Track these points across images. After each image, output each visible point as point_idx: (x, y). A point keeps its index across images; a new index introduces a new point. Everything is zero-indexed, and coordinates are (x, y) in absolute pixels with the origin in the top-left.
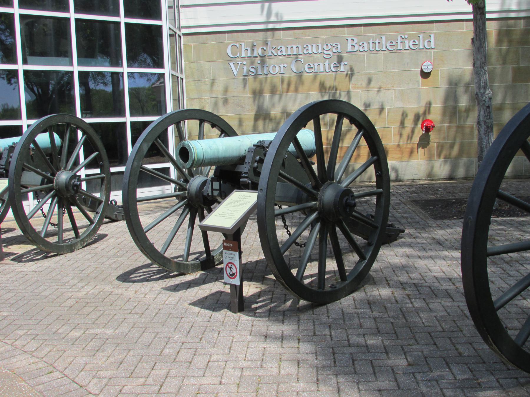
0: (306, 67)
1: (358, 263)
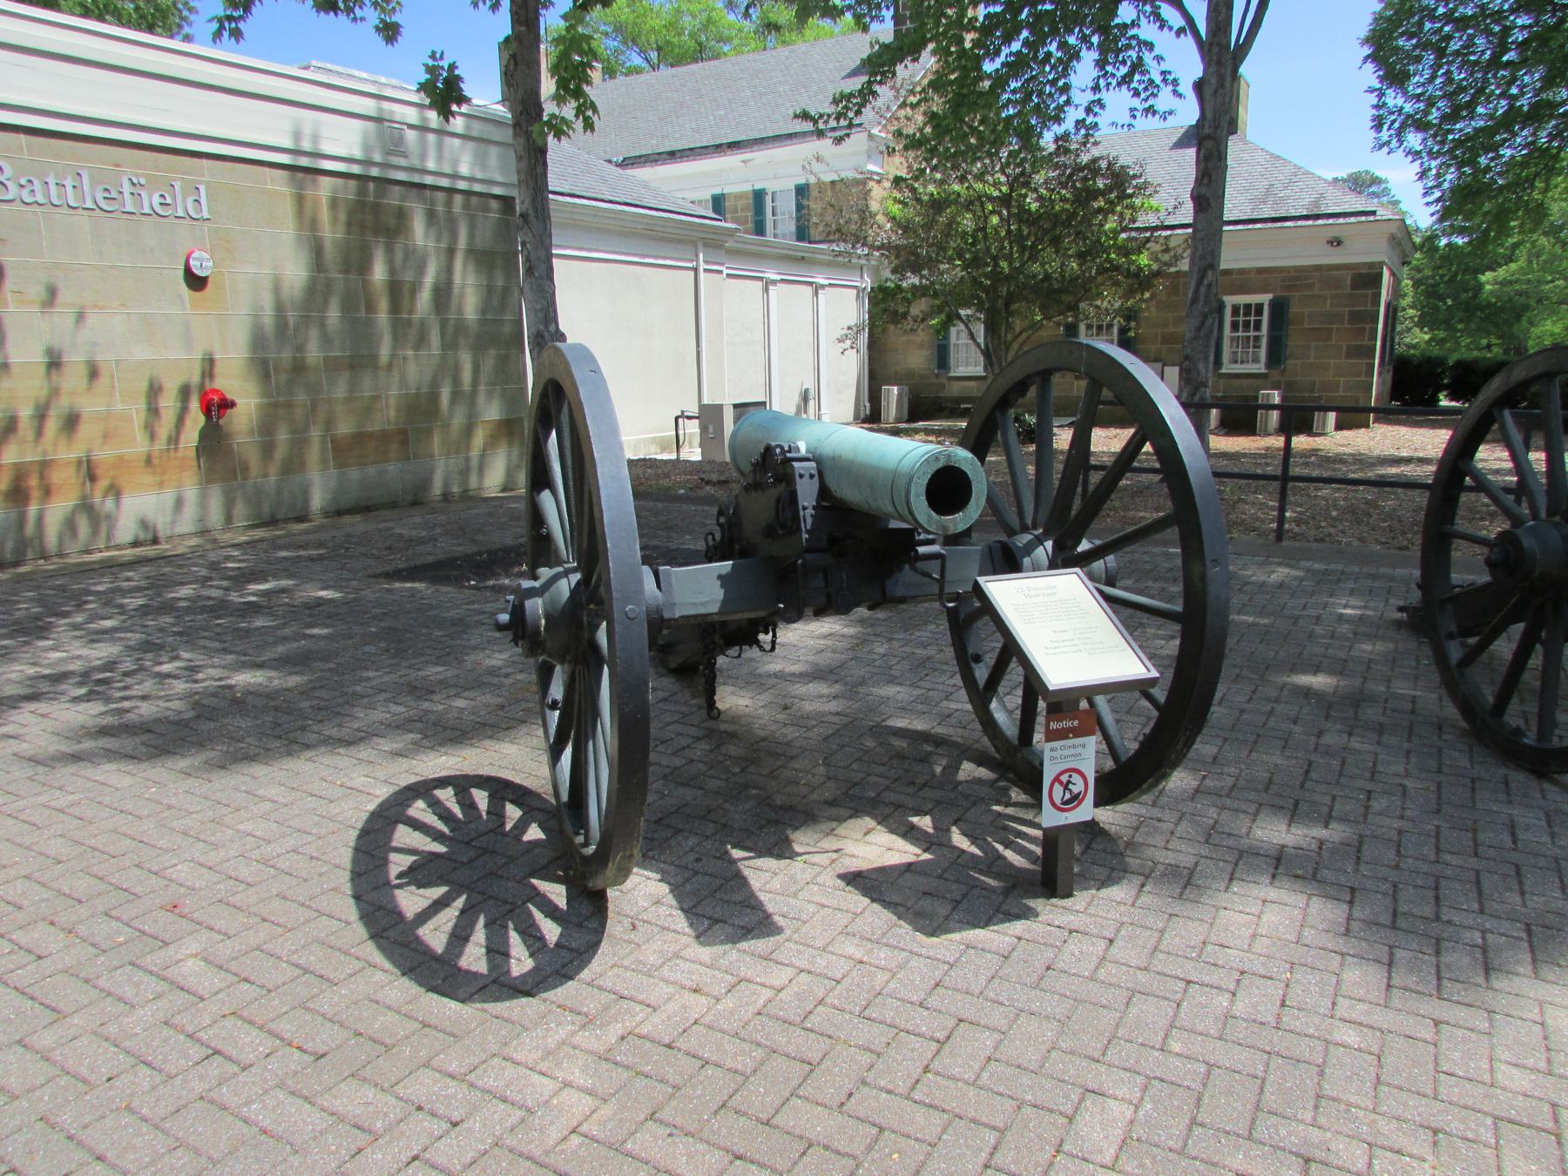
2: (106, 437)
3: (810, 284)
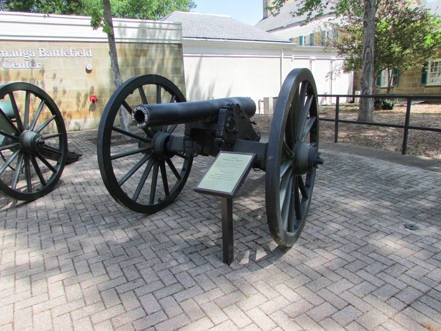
0: (13, 65)
1: (53, 175)
2: (67, 107)
3: (330, 59)
